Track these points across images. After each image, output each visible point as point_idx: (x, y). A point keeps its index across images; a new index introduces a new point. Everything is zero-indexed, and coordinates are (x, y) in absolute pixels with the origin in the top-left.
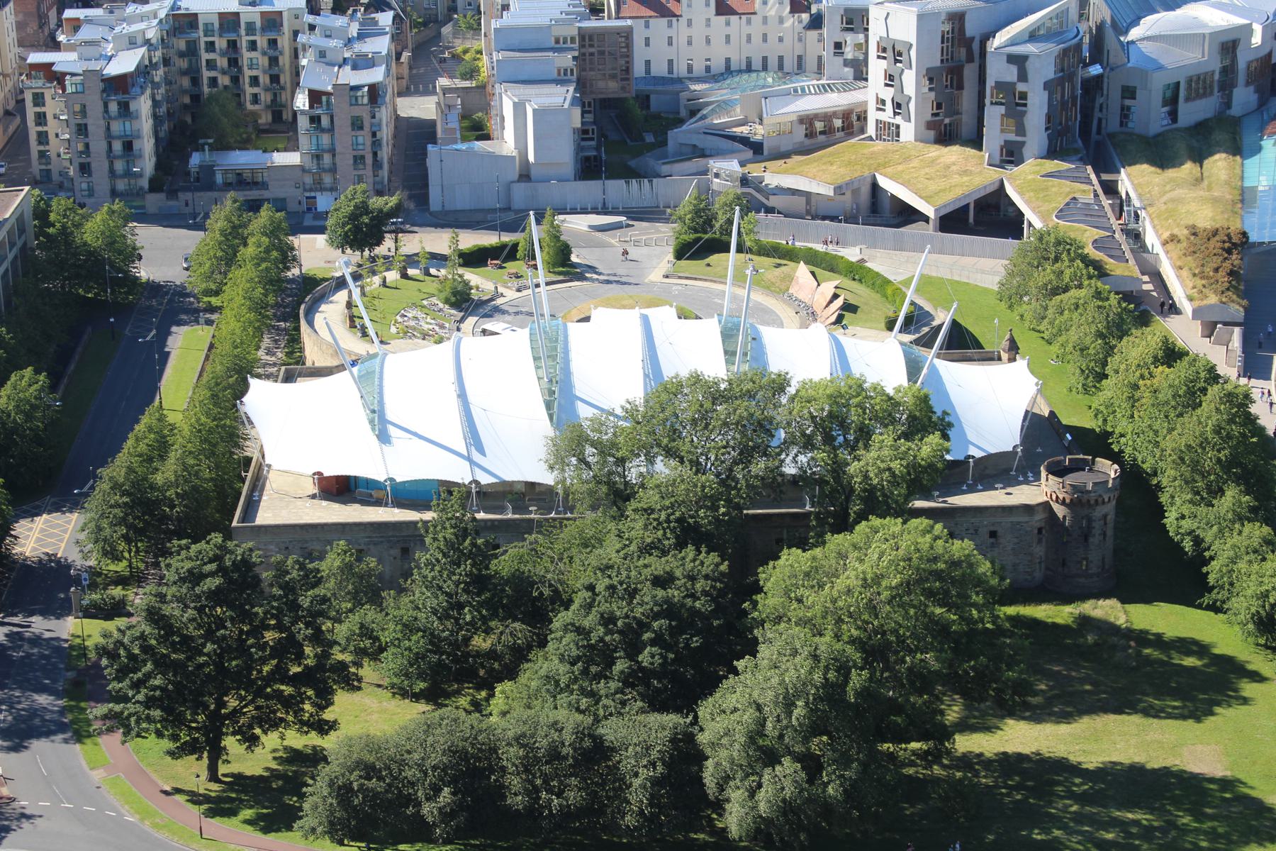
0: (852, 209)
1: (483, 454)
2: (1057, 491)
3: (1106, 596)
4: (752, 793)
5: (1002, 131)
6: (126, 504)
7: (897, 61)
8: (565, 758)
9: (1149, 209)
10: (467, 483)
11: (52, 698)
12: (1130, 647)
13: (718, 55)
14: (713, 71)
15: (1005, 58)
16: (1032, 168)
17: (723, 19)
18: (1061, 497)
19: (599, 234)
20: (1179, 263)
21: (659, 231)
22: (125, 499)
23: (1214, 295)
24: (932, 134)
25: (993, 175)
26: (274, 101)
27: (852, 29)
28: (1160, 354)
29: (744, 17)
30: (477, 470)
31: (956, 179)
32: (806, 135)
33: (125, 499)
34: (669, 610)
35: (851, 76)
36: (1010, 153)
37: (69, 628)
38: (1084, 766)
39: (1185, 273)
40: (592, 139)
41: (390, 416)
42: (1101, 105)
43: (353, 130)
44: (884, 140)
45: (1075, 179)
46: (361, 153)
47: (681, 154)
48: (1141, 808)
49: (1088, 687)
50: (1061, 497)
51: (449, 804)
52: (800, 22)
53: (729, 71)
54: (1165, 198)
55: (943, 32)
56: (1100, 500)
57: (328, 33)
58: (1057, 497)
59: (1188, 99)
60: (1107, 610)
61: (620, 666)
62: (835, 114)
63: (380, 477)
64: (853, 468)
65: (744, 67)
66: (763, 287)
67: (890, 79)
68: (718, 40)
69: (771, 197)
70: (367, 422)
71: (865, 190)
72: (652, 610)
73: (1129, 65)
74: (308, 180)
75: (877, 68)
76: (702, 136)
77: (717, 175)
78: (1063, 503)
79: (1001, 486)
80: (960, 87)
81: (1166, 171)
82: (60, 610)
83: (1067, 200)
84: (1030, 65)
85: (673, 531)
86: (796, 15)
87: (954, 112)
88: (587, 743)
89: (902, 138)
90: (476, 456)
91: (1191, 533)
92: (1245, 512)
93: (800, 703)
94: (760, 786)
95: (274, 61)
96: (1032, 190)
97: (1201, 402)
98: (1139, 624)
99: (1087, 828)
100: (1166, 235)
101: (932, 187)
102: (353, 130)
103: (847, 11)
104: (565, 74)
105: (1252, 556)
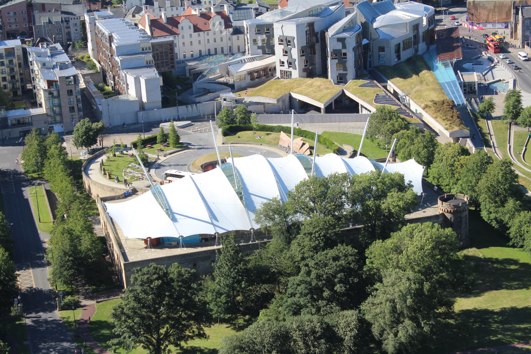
0: (283, 108)
1: (218, 221)
2: (447, 208)
3: (471, 247)
4: (396, 335)
5: (337, 70)
6: (72, 260)
7: (288, 45)
8: (318, 332)
9: (409, 95)
11: (69, 343)
12: (489, 265)
13: (196, 49)
16: (351, 83)
17: (197, 33)
18: (449, 210)
19: (182, 130)
20: (434, 116)
22: (71, 258)
23: (456, 127)
24: (305, 74)
25: (336, 90)
26: (13, 87)
27: (260, 33)
28: (460, 151)
30: (216, 228)
31: (325, 91)
32: (251, 79)
33: (71, 258)
34: (343, 269)
35: (261, 53)
36: (341, 79)
37: (58, 315)
38: (495, 311)
39: (439, 119)
41: (174, 210)
42: (370, 55)
43: (68, 96)
44: (285, 78)
45: (372, 86)
46: (72, 105)
47: (200, 93)
48: (525, 323)
49: (480, 282)
50: (449, 210)
54: (414, 90)
55: (306, 31)
56: (464, 209)
57: (39, 55)
58: (448, 210)
59: (404, 49)
60: (472, 252)
63: (177, 236)
64: (383, 206)
65: (207, 53)
67: (286, 53)
68: (195, 43)
69: (249, 106)
70: (166, 214)
71: (287, 99)
72: (336, 270)
73: (380, 38)
74: (50, 119)
75: (279, 49)
76: (208, 84)
77: (225, 100)
78: (450, 212)
79: (421, 209)
80: (315, 53)
81: (407, 80)
82: (51, 308)
83: (375, 95)
84: (347, 42)
85: (322, 240)
86: (227, 29)
87: (313, 64)
88: (324, 326)
90: (215, 222)
91: (496, 219)
92: (518, 208)
93: (408, 297)
94: (398, 332)
95: (12, 70)
96: (359, 93)
97: (487, 167)
98: (488, 256)
99: (509, 333)
100: (423, 105)
101: (318, 96)
102: (68, 96)
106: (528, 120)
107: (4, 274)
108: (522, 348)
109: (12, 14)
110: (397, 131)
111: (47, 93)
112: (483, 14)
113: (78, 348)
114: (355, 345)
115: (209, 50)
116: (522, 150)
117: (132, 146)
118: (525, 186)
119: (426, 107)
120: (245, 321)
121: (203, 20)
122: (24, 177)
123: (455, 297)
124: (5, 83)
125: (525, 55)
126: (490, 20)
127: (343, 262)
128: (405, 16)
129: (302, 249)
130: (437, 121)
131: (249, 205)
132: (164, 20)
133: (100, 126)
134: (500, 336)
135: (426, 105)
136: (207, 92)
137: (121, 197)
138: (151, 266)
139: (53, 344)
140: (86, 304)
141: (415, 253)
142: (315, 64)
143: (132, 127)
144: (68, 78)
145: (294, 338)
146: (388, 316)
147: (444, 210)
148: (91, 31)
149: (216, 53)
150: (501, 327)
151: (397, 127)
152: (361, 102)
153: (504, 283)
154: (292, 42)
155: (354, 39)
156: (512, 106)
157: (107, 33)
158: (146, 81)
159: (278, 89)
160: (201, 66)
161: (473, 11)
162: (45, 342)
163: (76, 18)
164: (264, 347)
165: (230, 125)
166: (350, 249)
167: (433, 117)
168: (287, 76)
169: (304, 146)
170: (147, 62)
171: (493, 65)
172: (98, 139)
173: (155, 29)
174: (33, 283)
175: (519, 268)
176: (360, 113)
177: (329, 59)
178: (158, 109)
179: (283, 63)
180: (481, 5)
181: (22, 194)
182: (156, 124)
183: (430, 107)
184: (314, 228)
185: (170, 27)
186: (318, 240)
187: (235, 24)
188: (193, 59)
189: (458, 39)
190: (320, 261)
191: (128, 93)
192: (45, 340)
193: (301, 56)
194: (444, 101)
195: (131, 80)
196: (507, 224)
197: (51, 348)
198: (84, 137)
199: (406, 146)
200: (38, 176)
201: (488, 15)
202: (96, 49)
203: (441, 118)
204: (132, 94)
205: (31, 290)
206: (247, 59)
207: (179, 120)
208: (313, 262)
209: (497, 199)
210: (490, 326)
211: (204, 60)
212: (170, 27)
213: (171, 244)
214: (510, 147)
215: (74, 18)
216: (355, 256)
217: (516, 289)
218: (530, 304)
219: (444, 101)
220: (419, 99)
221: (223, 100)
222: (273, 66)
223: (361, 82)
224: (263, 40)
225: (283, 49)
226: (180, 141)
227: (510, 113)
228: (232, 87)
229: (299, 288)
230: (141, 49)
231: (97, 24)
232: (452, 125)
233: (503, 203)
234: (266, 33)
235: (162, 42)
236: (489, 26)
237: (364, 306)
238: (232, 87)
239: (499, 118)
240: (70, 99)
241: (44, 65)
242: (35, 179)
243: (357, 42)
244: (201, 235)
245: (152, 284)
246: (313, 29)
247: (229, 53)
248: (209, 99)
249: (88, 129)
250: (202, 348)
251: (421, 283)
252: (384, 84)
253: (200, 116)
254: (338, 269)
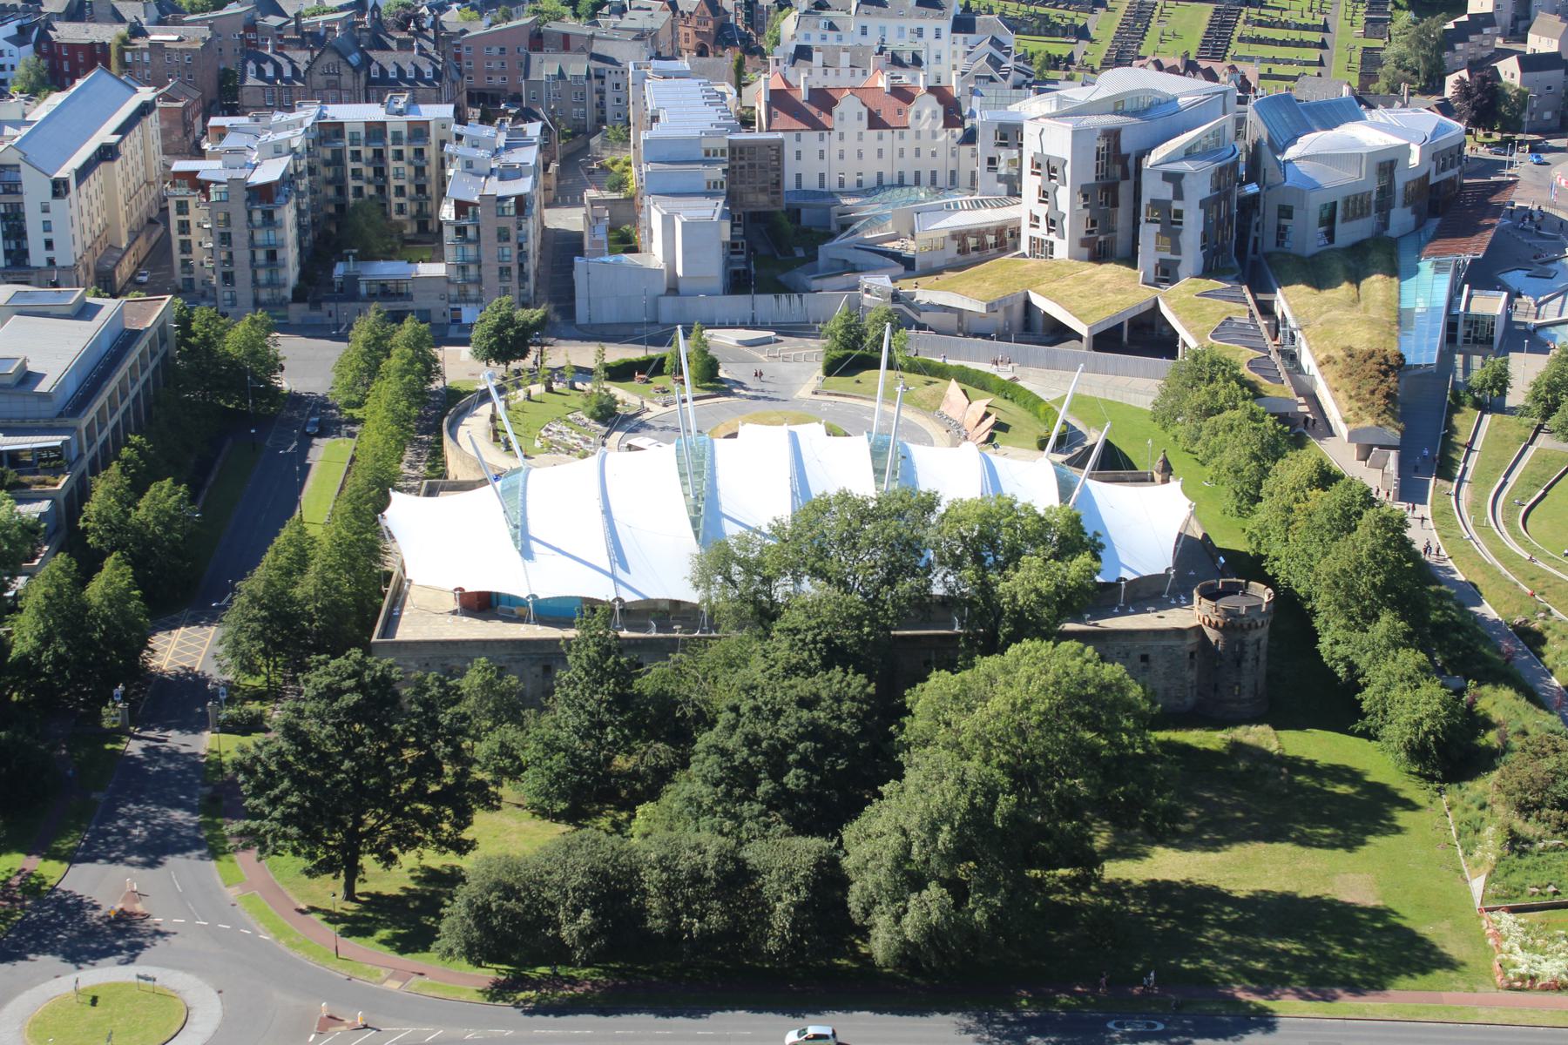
4: (898, 919)
5: (1157, 249)
6: (264, 618)
7: (1051, 177)
8: (708, 881)
12: (1282, 774)
13: (870, 169)
14: (865, 186)
16: (1187, 287)
17: (875, 133)
18: (1214, 620)
19: (747, 349)
20: (1335, 385)
21: (809, 348)
24: (1086, 251)
26: (420, 211)
27: (1006, 145)
28: (1315, 477)
29: (897, 131)
30: (621, 587)
31: (1111, 297)
32: (959, 252)
35: (1005, 192)
36: (1165, 272)
40: (741, 253)
41: (534, 530)
42: (1258, 224)
46: (508, 264)
47: (832, 269)
50: (1214, 620)
52: (954, 137)
59: (1345, 219)
60: (1260, 736)
61: (765, 787)
62: (988, 231)
63: (523, 594)
65: (896, 181)
71: (1018, 308)
72: (796, 731)
74: (453, 291)
75: (1031, 184)
76: (854, 251)
77: (868, 291)
78: (1216, 627)
80: (1115, 204)
82: (196, 724)
84: (1185, 183)
85: (819, 652)
87: (1109, 229)
89: (1056, 255)
90: (620, 573)
94: (906, 911)
95: (420, 171)
98: (1291, 751)
100: (1322, 356)
101: (1086, 305)
103: (1002, 126)
104: (715, 187)
108: (1249, 1002)
109: (495, 51)
118: (1480, 587)
122: (334, 415)
123: (1153, 844)
124: (401, 200)
129: (772, 666)
130: (1334, 399)
132: (802, 95)
142: (1113, 231)
144: (504, 199)
149: (917, 183)
150: (1227, 938)
153: (1297, 826)
154: (1059, 172)
156: (1548, 385)
158: (684, 224)
162: (137, 802)
164: (566, 895)
170: (709, 183)
173: (779, 113)
175: (1357, 793)
179: (1037, 219)
185: (814, 110)
188: (862, 190)
189: (1497, 211)
212: (814, 110)
214: (1504, 484)
218: (1328, 891)
230: (703, 152)
246: (1117, 146)
248: (845, 286)
249: (508, 321)
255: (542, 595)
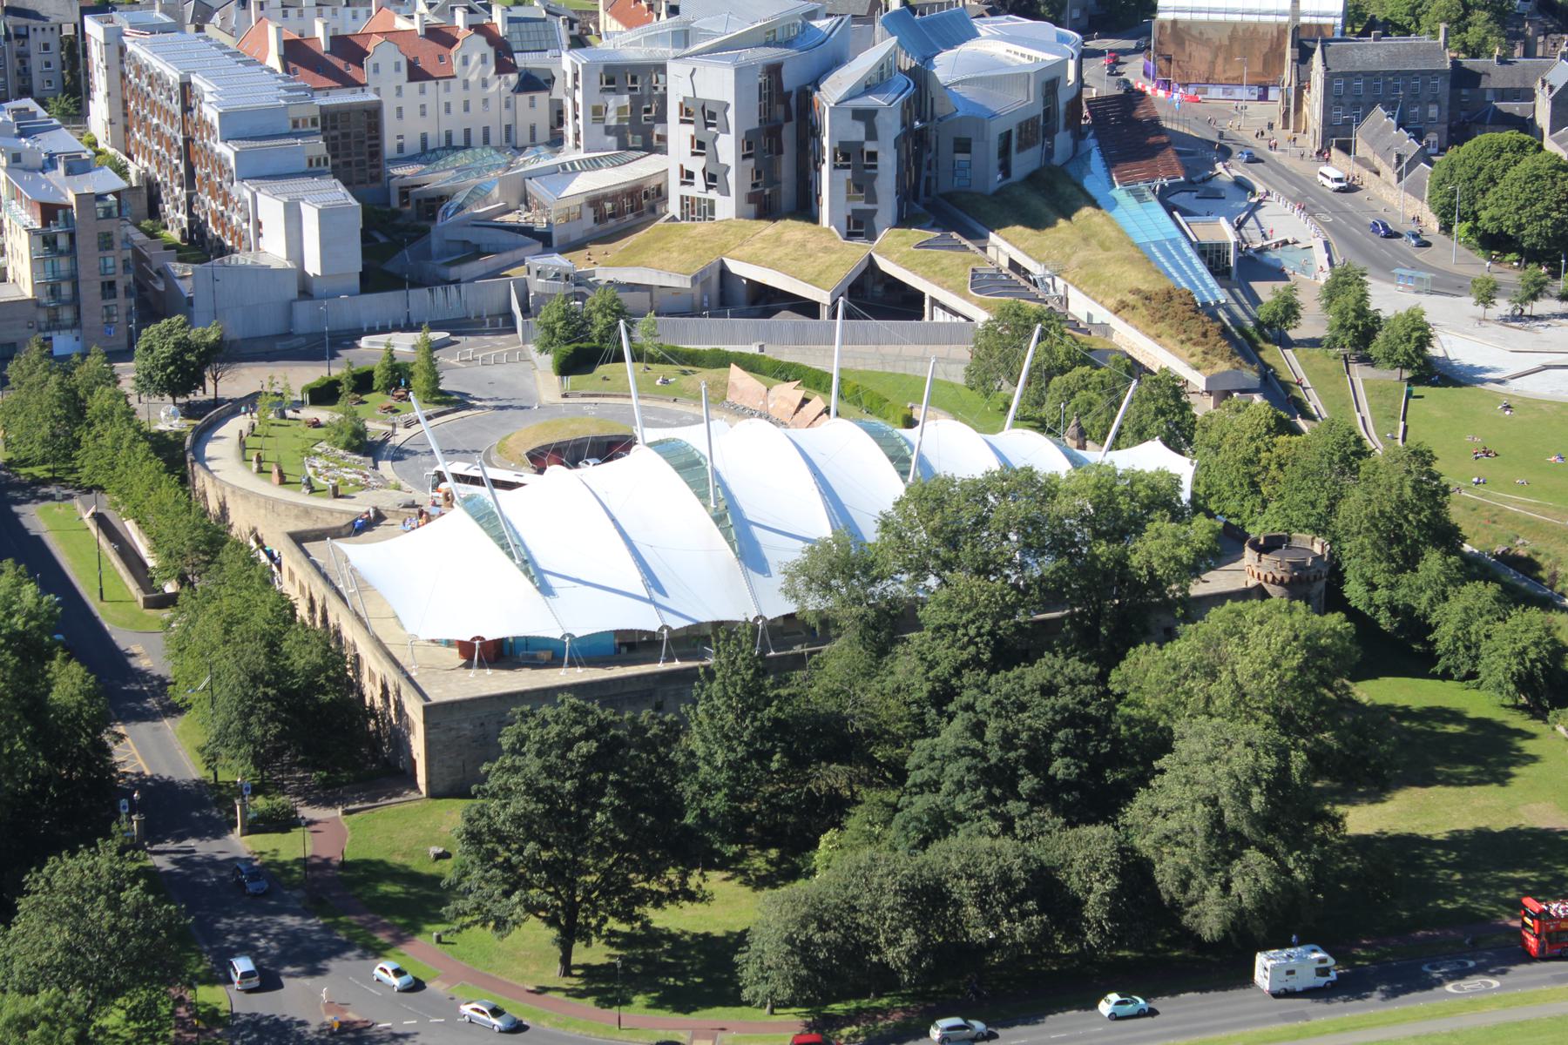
0: (702, 302)
1: (666, 595)
2: (1274, 571)
4: (1226, 887)
5: (848, 199)
7: (707, 125)
8: (1017, 881)
9: (1065, 275)
10: (751, 620)
11: (298, 918)
14: (431, 146)
15: (850, 114)
17: (416, 85)
18: (1278, 576)
20: (1153, 332)
21: (495, 347)
24: (752, 208)
25: (857, 252)
28: (1272, 423)
29: (441, 82)
30: (665, 613)
31: (825, 259)
33: (271, 692)
35: (615, 145)
36: (858, 224)
39: (1164, 339)
41: (543, 565)
42: (930, 162)
44: (693, 219)
45: (951, 247)
46: (111, 278)
47: (450, 254)
48: (1522, 868)
50: (1278, 576)
51: (915, 945)
52: (507, 84)
53: (450, 147)
54: (1074, 260)
58: (1274, 577)
59: (1020, 148)
61: (1027, 784)
62: (605, 198)
64: (1135, 560)
65: (443, 144)
66: (691, 397)
67: (699, 146)
68: (411, 112)
70: (521, 574)
72: (1053, 720)
75: (679, 135)
78: (1281, 583)
80: (780, 151)
82: (220, 829)
84: (879, 121)
86: (503, 76)
87: (773, 181)
89: (719, 215)
90: (659, 598)
97: (1358, 467)
100: (1112, 302)
101: (810, 269)
103: (608, 68)
105: (1487, 617)
106: (1401, 349)
107: (89, 730)
110: (1062, 371)
111: (39, 240)
112: (1199, 58)
113: (326, 929)
114: (1113, 914)
115: (449, 135)
116: (1397, 428)
117: (307, 397)
119: (1120, 308)
120: (769, 862)
121: (433, 46)
125: (1338, 175)
126: (1219, 75)
127: (1068, 697)
128: (1012, 55)
130: (1163, 345)
131: (751, 556)
133: (212, 337)
134: (1462, 900)
135: (1122, 302)
136: (475, 252)
137: (344, 532)
138: (563, 701)
139: (255, 920)
140: (316, 818)
141: (1257, 676)
143: (279, 345)
144: (100, 197)
145: (956, 896)
146: (1200, 841)
147: (1262, 577)
148: (107, 68)
149: (467, 145)
151: (1062, 357)
152: (929, 289)
155: (898, 113)
157: (173, 75)
159: (686, 249)
160: (437, 178)
161: (1170, 49)
163: (48, 29)
165: (577, 345)
166: (1076, 667)
167: (1148, 335)
168: (699, 214)
169: (807, 406)
170: (310, 162)
171: (1254, 200)
172: (208, 374)
173: (299, 69)
174: (140, 761)
176: (927, 318)
177: (825, 169)
178: (351, 295)
179: (690, 175)
180: (1195, 32)
181: (20, 525)
182: (348, 338)
183: (1134, 308)
184: (962, 611)
185: (339, 63)
186: (976, 644)
187: (523, 61)
190: (1007, 697)
191: (258, 248)
192: (226, 909)
193: (745, 157)
194: (1169, 293)
195: (271, 209)
196: (1425, 617)
197: (251, 931)
198: (172, 368)
199: (1094, 410)
200: (50, 475)
201: (1213, 63)
202: (120, 121)
203: (1172, 337)
204: (273, 249)
205: (140, 780)
206: (578, 161)
207: (409, 327)
208: (989, 699)
209: (1396, 550)
210: (1432, 875)
211: (442, 162)
212: (339, 63)
213: (534, 657)
215: (43, 29)
216: (1094, 683)
217: (1471, 783)
219: (1169, 293)
220: (1096, 284)
221: (533, 272)
222: (653, 184)
223: (917, 235)
224: (621, 110)
225: (693, 137)
226: (441, 388)
227: (1349, 329)
228: (545, 240)
229: (950, 768)
231: (130, 47)
232: (1209, 357)
233: (1411, 561)
234: (631, 89)
235: (350, 105)
236: (1215, 92)
237: (1134, 812)
238: (545, 240)
239: (1314, 343)
240: (105, 258)
241: (16, 158)
242: (45, 483)
243: (904, 124)
244: (617, 633)
245: (571, 749)
247: (504, 144)
248: (483, 272)
250: (673, 930)
251: (1283, 753)
252: (981, 242)
253: (467, 318)
254: (1058, 718)
255: (579, 633)
